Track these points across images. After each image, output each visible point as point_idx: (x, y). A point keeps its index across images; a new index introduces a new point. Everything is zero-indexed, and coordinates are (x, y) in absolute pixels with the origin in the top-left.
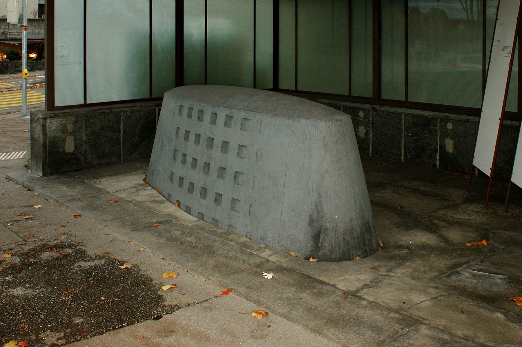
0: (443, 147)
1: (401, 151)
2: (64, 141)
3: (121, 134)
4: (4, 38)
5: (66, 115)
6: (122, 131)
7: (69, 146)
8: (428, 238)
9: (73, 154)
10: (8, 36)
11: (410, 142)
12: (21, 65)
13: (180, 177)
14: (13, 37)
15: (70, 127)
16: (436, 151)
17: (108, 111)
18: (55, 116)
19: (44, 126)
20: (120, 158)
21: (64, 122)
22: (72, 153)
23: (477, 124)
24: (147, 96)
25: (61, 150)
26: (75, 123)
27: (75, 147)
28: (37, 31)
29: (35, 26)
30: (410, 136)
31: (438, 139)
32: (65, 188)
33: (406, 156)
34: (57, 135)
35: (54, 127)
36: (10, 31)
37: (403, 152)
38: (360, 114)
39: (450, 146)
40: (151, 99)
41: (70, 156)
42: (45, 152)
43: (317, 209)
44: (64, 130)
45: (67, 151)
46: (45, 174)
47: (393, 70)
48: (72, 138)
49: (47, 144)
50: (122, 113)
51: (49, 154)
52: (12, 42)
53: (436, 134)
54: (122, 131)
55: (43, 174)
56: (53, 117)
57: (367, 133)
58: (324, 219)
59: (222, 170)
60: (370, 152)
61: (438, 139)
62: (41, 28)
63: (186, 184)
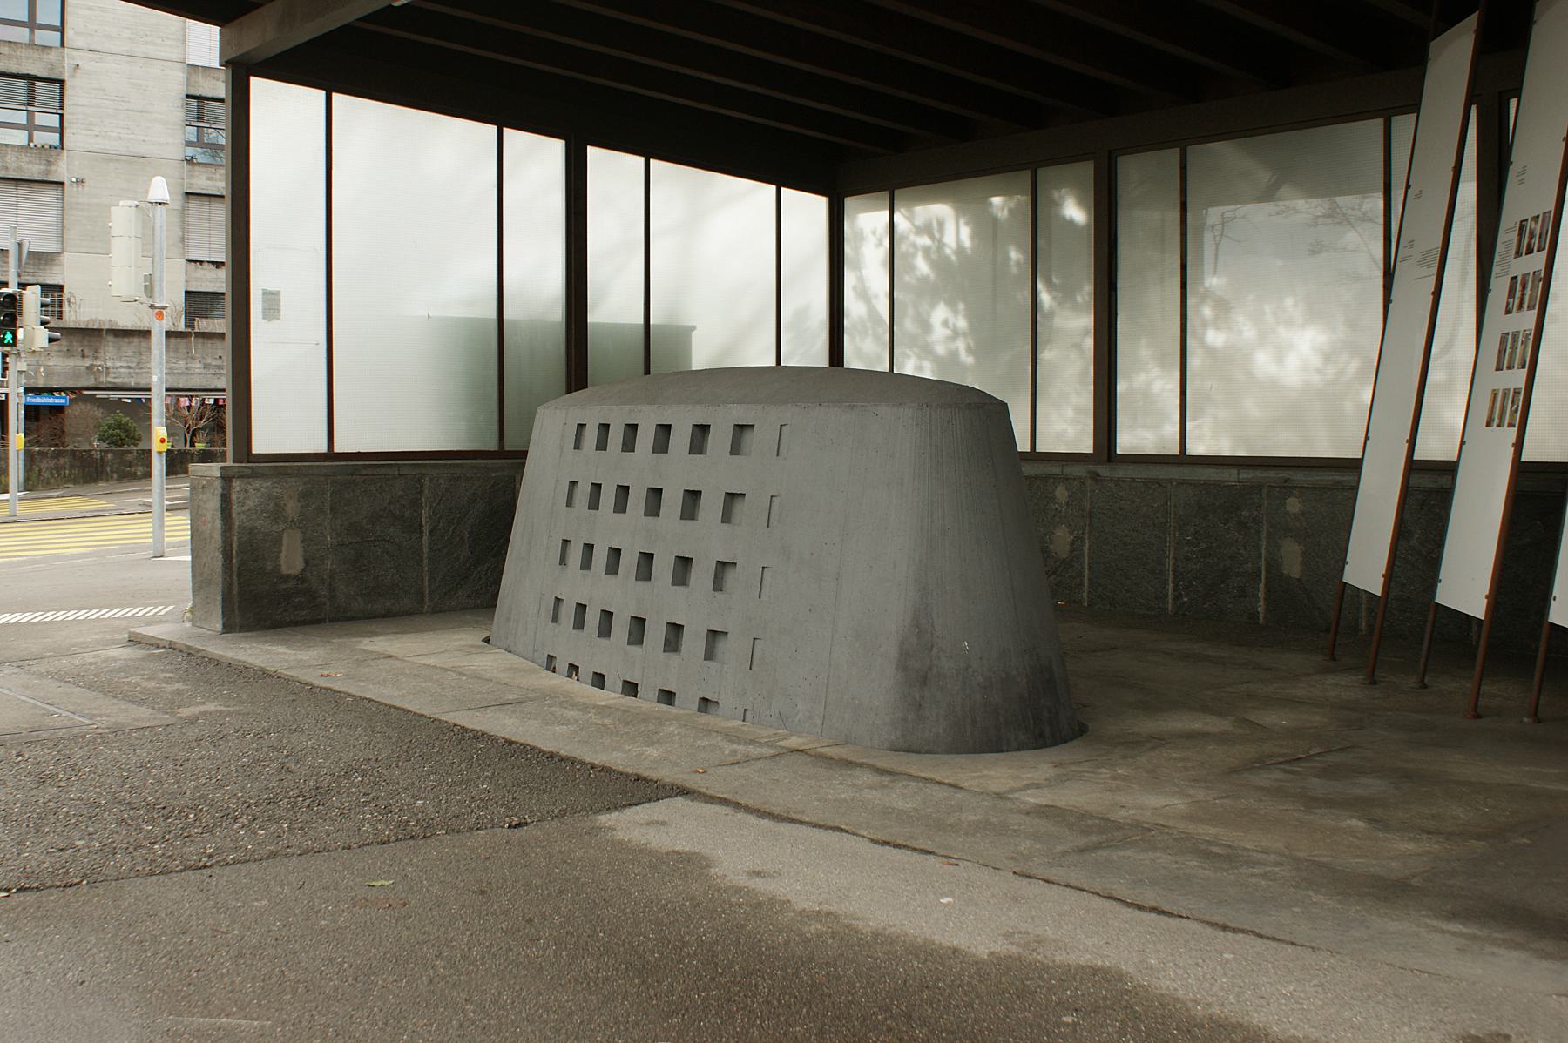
0: (1274, 565)
1: (1165, 584)
2: (277, 542)
3: (425, 538)
4: (91, 382)
5: (281, 474)
6: (426, 530)
7: (291, 559)
8: (1018, 263)
9: (301, 578)
10: (103, 379)
11: (1188, 559)
12: (149, 418)
13: (579, 605)
14: (118, 380)
15: (292, 508)
16: (1256, 576)
17: (390, 471)
18: (255, 475)
19: (226, 499)
20: (422, 602)
21: (277, 491)
22: (296, 577)
23: (1355, 489)
24: (493, 446)
25: (269, 566)
26: (305, 496)
27: (307, 562)
28: (182, 364)
29: (176, 350)
30: (1189, 543)
31: (1264, 543)
32: (281, 649)
33: (1177, 598)
34: (258, 524)
35: (251, 503)
36: (109, 364)
37: (1171, 586)
38: (1057, 493)
39: (1292, 559)
40: (501, 453)
41: (290, 585)
42: (227, 566)
43: (917, 626)
44: (277, 512)
45: (285, 570)
46: (228, 628)
47: (1146, 380)
48: (298, 535)
49: (235, 545)
50: (426, 481)
51: (239, 575)
52: (114, 395)
53: (1258, 532)
54: (426, 530)
55: (224, 626)
56: (248, 476)
57: (1076, 545)
58: (935, 650)
59: (684, 563)
60: (1085, 595)
61: (1264, 543)
62: (193, 358)
63: (593, 619)
